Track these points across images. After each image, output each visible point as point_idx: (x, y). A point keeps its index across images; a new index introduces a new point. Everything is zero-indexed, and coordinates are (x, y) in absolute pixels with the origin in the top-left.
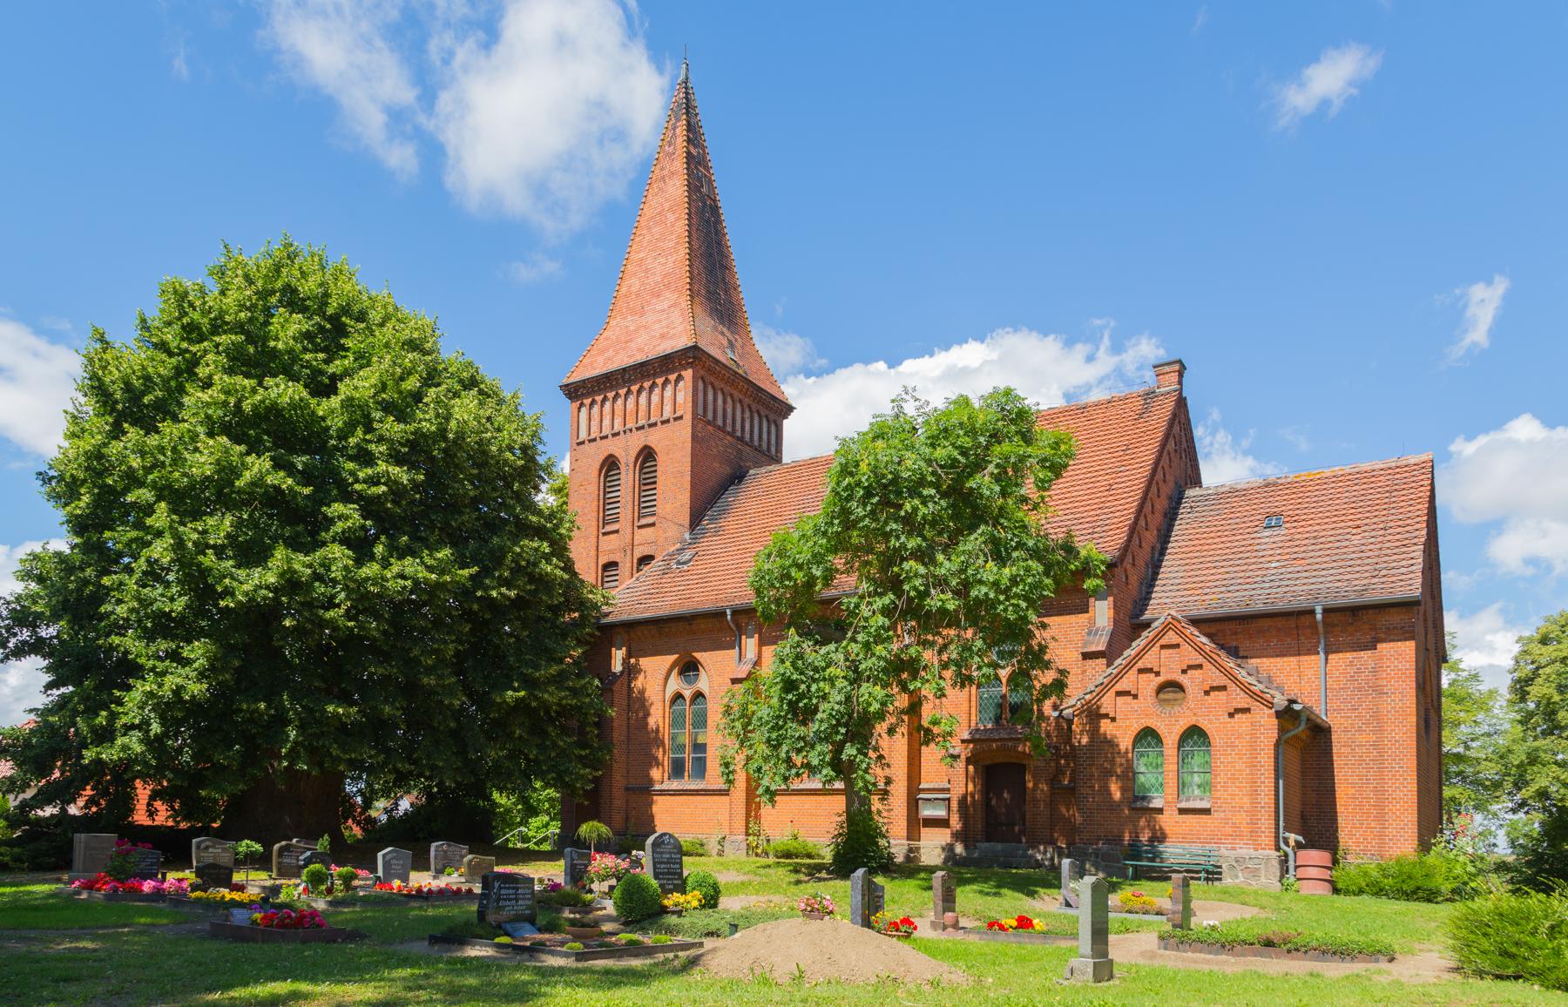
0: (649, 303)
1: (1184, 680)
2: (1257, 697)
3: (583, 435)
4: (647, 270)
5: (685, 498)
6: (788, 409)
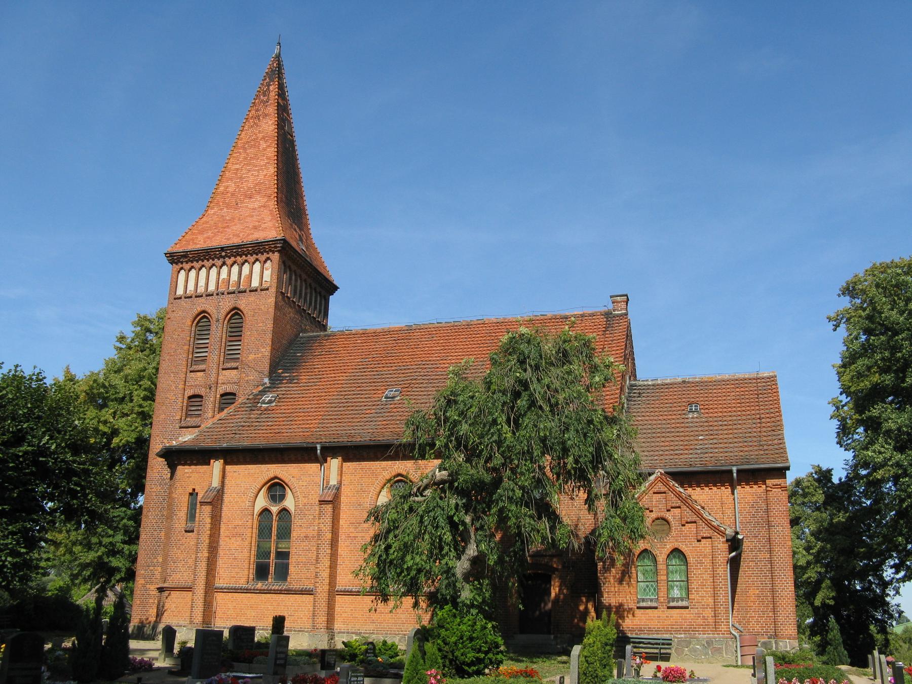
0: (242, 202)
1: (669, 516)
2: (716, 529)
3: (180, 292)
4: (241, 178)
5: (266, 351)
6: (332, 288)
